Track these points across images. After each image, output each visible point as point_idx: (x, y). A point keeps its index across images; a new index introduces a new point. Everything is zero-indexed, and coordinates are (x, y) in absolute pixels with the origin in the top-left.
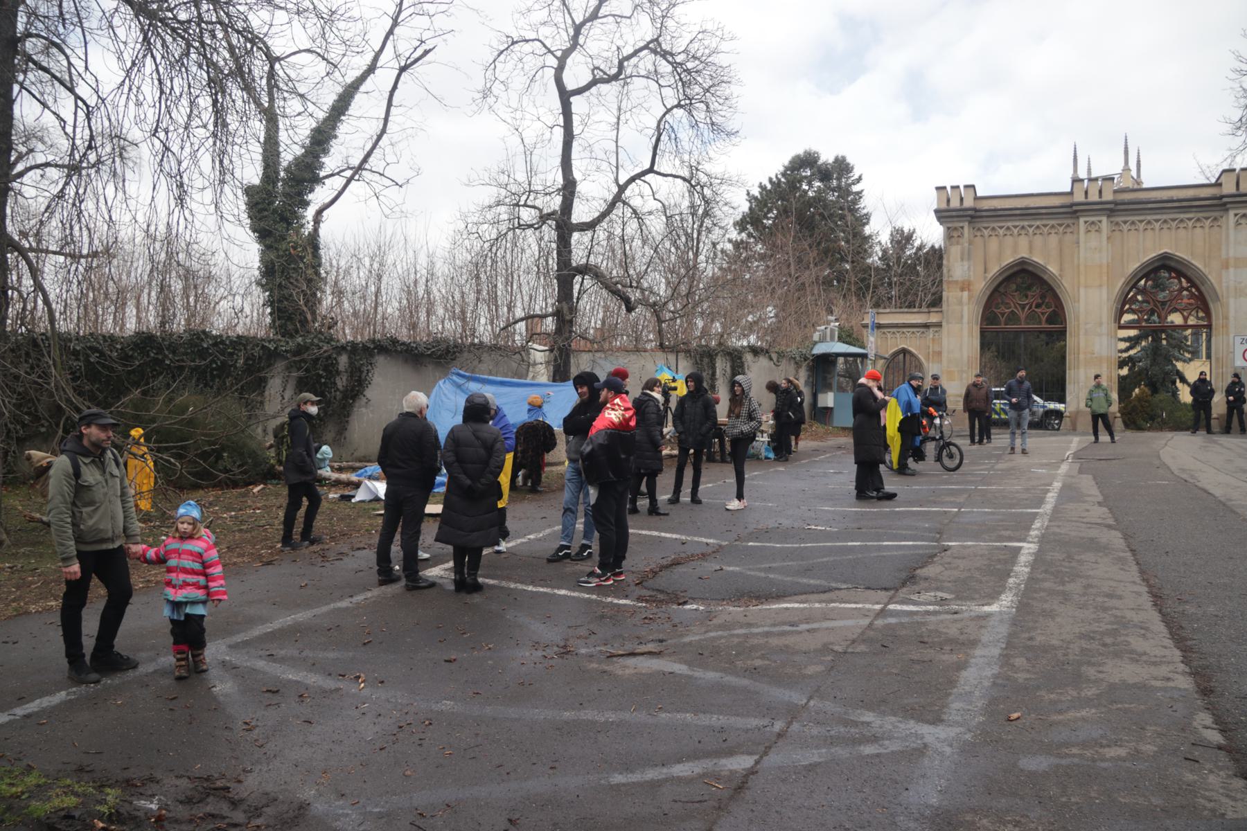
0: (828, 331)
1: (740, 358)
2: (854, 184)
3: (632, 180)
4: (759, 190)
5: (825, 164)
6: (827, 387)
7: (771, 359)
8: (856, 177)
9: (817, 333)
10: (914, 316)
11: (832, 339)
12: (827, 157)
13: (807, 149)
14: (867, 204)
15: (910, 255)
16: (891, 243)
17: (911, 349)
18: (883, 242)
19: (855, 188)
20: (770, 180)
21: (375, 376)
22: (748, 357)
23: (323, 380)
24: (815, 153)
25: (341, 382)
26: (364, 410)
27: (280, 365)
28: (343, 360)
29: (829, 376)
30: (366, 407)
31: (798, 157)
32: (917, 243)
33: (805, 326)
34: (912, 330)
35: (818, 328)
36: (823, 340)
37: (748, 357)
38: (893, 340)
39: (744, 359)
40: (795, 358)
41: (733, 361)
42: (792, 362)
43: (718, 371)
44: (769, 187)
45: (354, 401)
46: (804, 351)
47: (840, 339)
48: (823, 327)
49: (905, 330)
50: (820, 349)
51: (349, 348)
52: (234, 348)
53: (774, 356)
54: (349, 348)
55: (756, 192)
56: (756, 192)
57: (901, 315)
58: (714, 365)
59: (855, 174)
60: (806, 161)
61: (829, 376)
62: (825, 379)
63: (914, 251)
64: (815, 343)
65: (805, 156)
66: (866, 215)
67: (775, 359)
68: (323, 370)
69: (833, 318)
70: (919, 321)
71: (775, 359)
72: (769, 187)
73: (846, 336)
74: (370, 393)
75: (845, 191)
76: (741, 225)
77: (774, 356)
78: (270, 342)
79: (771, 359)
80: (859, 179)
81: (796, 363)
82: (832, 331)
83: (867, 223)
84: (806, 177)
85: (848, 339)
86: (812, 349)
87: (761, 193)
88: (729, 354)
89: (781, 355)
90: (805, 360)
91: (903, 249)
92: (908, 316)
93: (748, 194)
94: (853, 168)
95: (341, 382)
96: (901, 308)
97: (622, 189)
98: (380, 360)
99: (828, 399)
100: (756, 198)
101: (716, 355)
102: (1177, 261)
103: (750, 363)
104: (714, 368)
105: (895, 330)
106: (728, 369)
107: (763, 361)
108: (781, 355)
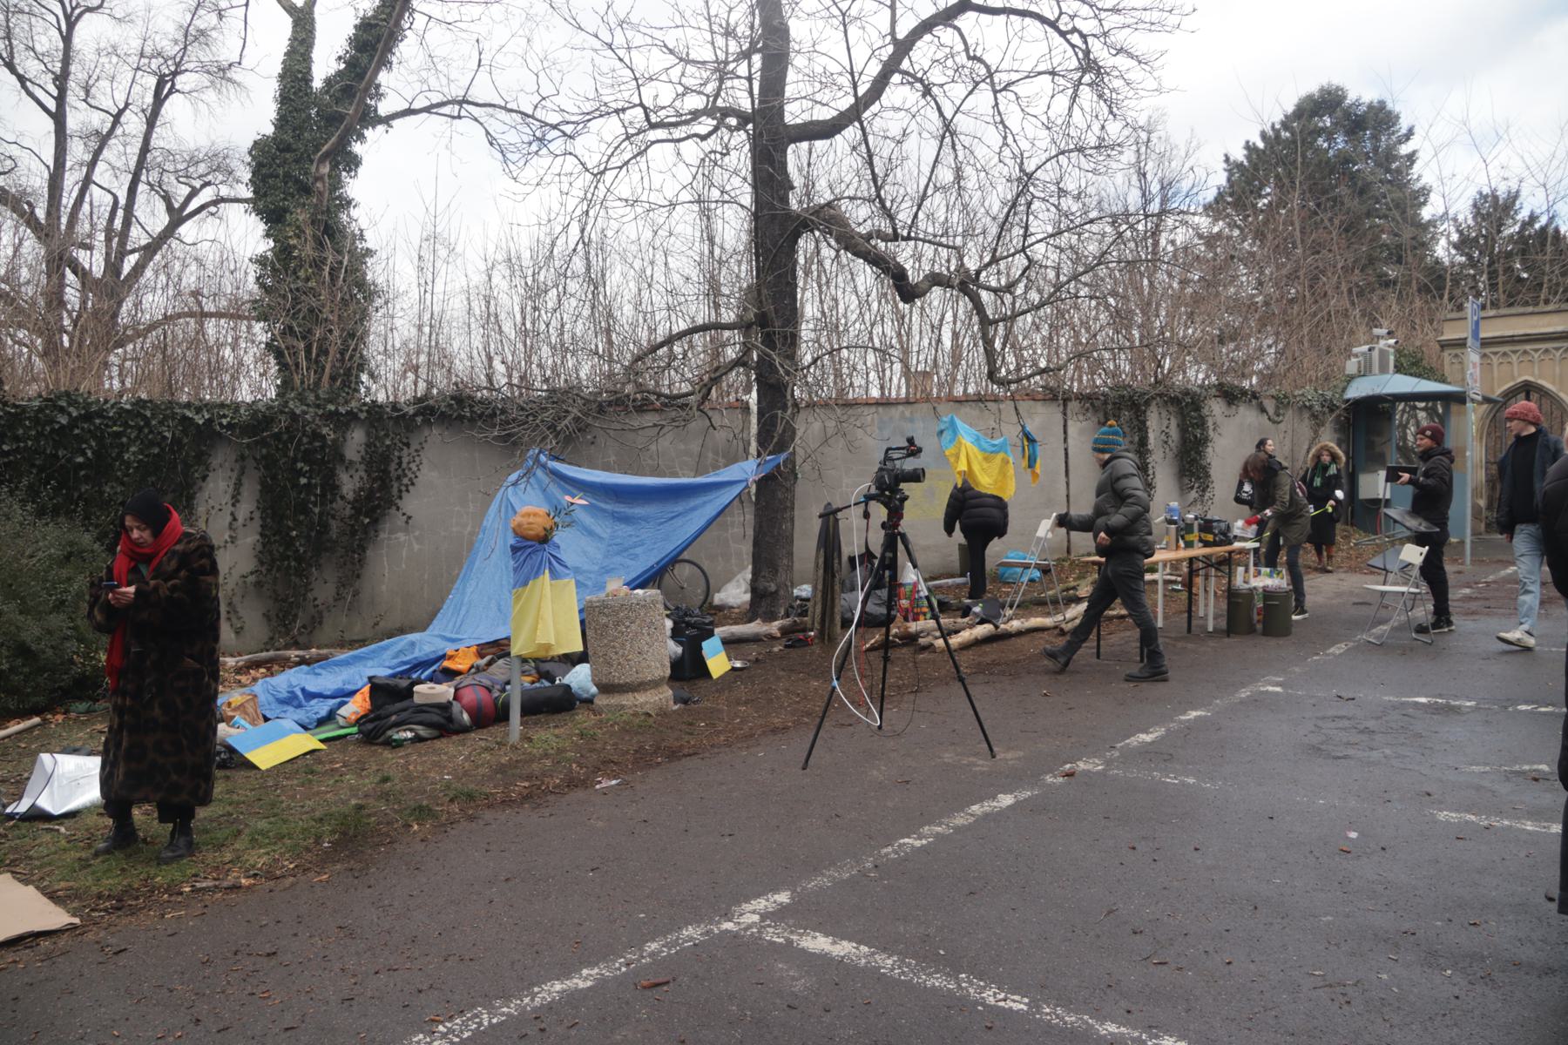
0: (1376, 354)
1: (1198, 409)
2: (1400, 142)
3: (926, 27)
4: (1245, 152)
5: (1357, 104)
6: (1376, 460)
7: (1263, 410)
8: (1404, 131)
9: (1354, 360)
10: (1546, 319)
11: (1383, 369)
12: (1361, 93)
13: (1325, 83)
14: (1423, 173)
15: (1512, 236)
16: (1475, 218)
17: (1540, 382)
18: (1461, 218)
19: (1404, 149)
20: (1264, 136)
21: (425, 469)
22: (1216, 408)
23: (303, 481)
24: (1338, 89)
25: (349, 484)
26: (401, 536)
27: (1153, 408)
28: (355, 441)
29: (1378, 440)
30: (406, 531)
31: (1310, 98)
32: (1524, 215)
33: (1329, 351)
34: (1543, 346)
35: (1355, 350)
36: (1365, 371)
37: (1216, 408)
38: (1505, 367)
39: (1205, 411)
40: (1310, 408)
41: (1182, 415)
42: (1306, 415)
43: (1151, 436)
44: (1261, 145)
45: (375, 521)
46: (1329, 394)
47: (1399, 369)
48: (1365, 348)
49: (1528, 347)
50: (1357, 390)
51: (363, 416)
52: (126, 425)
53: (1270, 405)
54: (363, 416)
55: (1239, 155)
56: (1239, 155)
57: (1521, 320)
58: (1144, 423)
59: (1403, 126)
60: (1327, 102)
61: (1378, 440)
62: (1370, 445)
63: (1517, 228)
64: (1351, 378)
65: (1322, 96)
66: (1424, 188)
67: (1271, 410)
68: (304, 460)
69: (1383, 331)
70: (1560, 328)
71: (1271, 410)
72: (1261, 145)
73: (1409, 363)
74: (411, 503)
75: (1387, 158)
76: (1215, 209)
77: (1270, 405)
78: (198, 410)
79: (1263, 410)
80: (1410, 133)
81: (1314, 416)
82: (1383, 353)
83: (1424, 203)
84: (1324, 129)
85: (1414, 369)
86: (1344, 390)
87: (1248, 157)
88: (1175, 401)
89: (1282, 402)
90: (1332, 411)
91: (1500, 225)
92: (1534, 320)
93: (1227, 160)
94: (1397, 117)
95: (349, 484)
96: (1511, 305)
97: (903, 47)
98: (434, 435)
99: (1375, 485)
100: (1239, 166)
101: (1147, 403)
102: (657, 563)
103: (1219, 419)
104: (1142, 429)
105: (1507, 349)
106: (1174, 432)
107: (1247, 415)
108: (1282, 402)
